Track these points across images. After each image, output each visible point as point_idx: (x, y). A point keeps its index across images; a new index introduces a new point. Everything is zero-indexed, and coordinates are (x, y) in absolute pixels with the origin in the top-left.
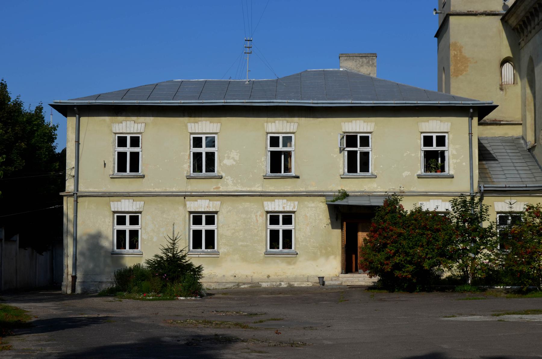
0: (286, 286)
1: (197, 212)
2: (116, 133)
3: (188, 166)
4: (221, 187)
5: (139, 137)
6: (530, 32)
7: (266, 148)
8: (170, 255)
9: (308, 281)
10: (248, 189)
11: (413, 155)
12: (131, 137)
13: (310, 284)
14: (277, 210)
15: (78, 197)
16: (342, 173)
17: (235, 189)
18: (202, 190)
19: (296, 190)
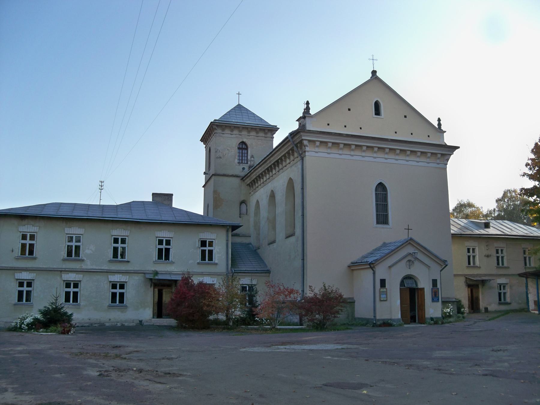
0: (120, 325)
2: (20, 232)
5: (35, 235)
8: (54, 307)
9: (133, 323)
10: (100, 268)
13: (134, 324)
14: (116, 280)
16: (155, 260)
17: (92, 267)
18: (72, 268)
19: (127, 269)
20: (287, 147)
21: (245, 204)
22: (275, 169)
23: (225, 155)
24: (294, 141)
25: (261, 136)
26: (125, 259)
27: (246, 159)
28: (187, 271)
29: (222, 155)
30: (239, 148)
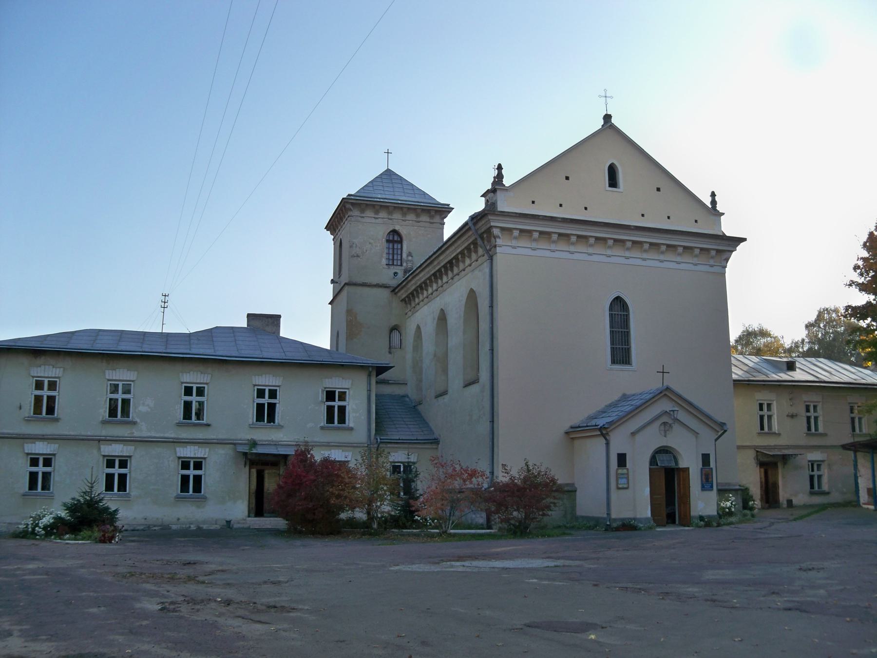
0: (195, 528)
2: (33, 377)
4: (135, 432)
6: (418, 304)
7: (181, 397)
8: (88, 498)
9: (216, 524)
10: (162, 435)
12: (49, 381)
13: (218, 527)
14: (188, 456)
16: (251, 423)
19: (207, 437)
21: (397, 332)
23: (365, 251)
25: (424, 222)
27: (399, 258)
28: (303, 441)
29: (360, 252)
30: (388, 241)
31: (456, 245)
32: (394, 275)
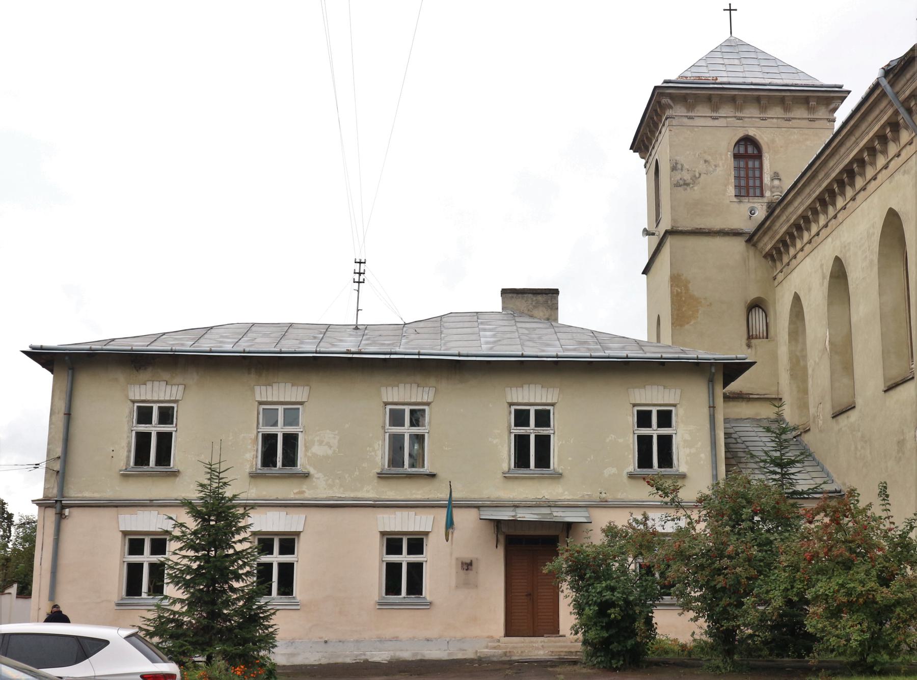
1: (277, 533)
2: (134, 402)
3: (254, 455)
7: (384, 427)
10: (352, 495)
11: (621, 440)
12: (159, 407)
15: (64, 507)
16: (506, 469)
20: (877, 118)
21: (761, 311)
22: (843, 193)
24: (898, 93)
25: (799, 119)
26: (422, 470)
27: (758, 183)
28: (598, 499)
30: (736, 156)
31: (857, 134)
32: (751, 212)
